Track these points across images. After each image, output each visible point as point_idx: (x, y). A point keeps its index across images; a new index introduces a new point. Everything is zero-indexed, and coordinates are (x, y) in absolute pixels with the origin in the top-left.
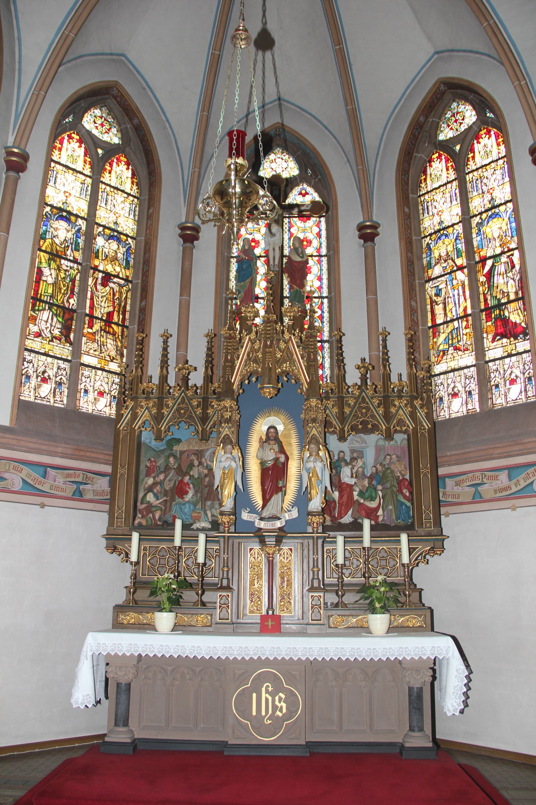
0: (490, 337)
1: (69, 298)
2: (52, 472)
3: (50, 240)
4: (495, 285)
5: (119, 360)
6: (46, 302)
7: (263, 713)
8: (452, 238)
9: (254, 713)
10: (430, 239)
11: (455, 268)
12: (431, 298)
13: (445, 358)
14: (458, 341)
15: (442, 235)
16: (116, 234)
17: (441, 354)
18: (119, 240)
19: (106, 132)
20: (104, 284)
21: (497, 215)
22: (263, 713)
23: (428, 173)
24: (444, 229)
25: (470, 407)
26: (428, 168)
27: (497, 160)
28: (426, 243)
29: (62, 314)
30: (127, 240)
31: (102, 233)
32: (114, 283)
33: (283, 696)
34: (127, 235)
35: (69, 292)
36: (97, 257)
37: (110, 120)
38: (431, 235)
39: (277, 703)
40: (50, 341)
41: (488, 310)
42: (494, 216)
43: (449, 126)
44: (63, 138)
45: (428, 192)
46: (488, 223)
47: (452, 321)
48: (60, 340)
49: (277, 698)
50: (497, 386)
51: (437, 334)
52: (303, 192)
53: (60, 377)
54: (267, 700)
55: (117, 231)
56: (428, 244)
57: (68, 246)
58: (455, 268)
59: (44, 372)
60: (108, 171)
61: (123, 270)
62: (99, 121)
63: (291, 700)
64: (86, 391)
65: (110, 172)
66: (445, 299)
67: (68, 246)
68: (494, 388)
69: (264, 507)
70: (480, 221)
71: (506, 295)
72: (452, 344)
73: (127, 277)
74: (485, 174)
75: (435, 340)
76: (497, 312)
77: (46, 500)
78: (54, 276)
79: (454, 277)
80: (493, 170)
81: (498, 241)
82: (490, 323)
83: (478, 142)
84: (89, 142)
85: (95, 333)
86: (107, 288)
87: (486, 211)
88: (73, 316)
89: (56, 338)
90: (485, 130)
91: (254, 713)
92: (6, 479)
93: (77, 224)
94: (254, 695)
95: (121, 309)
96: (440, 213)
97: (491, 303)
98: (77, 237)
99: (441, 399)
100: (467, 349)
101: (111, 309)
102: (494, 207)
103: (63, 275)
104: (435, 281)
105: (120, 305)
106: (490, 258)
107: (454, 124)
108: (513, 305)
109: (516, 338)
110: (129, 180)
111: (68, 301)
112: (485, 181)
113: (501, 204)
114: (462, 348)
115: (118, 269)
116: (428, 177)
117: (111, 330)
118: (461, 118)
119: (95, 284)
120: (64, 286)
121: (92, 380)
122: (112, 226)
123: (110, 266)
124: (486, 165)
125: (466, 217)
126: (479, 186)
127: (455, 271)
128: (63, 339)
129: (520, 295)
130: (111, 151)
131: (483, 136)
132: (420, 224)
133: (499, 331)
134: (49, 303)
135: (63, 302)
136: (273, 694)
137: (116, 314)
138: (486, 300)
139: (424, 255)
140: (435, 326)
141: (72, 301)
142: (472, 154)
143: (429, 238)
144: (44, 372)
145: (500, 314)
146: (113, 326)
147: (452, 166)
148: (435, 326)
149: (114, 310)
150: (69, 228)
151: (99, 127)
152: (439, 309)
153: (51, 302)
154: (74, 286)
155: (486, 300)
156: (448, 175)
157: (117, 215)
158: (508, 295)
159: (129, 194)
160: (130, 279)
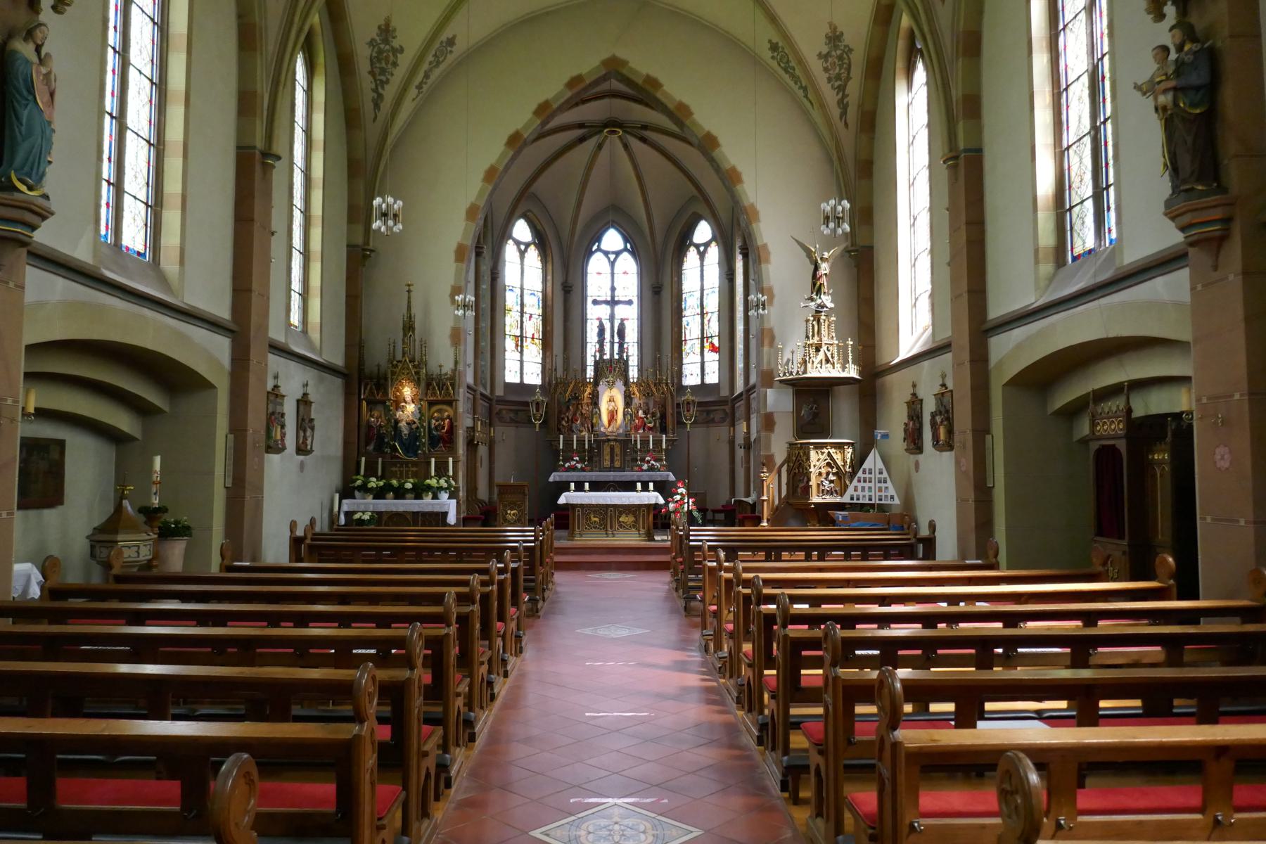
84: (518, 243)
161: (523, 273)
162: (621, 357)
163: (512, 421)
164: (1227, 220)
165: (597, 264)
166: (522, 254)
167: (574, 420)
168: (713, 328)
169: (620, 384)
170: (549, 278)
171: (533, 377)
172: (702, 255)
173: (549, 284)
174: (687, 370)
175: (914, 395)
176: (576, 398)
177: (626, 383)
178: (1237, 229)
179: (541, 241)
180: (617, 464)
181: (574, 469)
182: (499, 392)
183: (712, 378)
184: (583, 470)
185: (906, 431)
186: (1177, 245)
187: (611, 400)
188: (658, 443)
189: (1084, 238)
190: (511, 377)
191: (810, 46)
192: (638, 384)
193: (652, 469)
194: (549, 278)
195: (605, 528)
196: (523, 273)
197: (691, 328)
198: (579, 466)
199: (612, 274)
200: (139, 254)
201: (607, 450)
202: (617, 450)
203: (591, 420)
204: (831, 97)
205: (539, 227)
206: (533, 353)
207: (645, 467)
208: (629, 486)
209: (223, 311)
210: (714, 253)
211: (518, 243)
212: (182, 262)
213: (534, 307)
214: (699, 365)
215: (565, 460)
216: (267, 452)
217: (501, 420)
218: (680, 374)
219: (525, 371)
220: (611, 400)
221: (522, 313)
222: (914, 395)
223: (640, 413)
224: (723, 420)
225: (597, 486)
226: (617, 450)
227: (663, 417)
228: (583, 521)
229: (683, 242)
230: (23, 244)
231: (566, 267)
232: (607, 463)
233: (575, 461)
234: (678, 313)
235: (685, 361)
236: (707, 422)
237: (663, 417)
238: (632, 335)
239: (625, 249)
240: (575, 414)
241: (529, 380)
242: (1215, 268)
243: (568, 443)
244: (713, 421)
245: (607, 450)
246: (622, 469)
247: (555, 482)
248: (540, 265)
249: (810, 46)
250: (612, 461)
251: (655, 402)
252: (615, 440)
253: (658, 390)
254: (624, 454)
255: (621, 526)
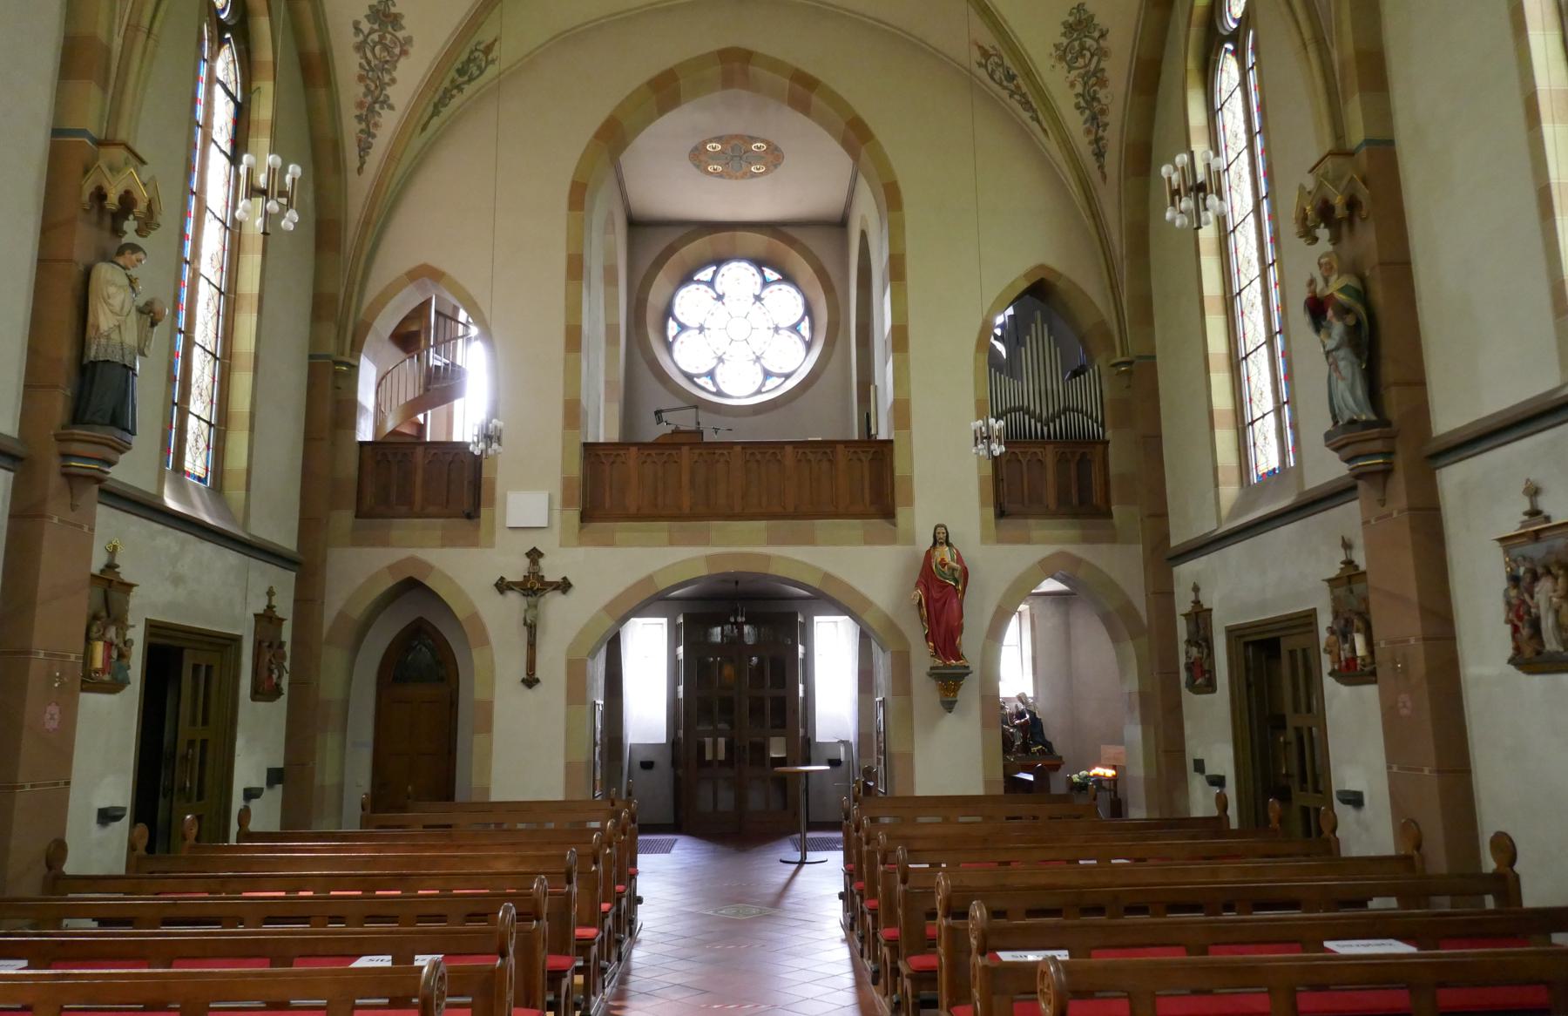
164: (1388, 454)
175: (1197, 602)
178: (1399, 461)
185: (1509, 603)
186: (1340, 478)
189: (1267, 457)
191: (1039, 39)
200: (199, 479)
204: (1075, 122)
209: (285, 537)
212: (248, 489)
216: (83, 690)
222: (1197, 602)
230: (99, 481)
242: (1383, 503)
249: (1039, 39)
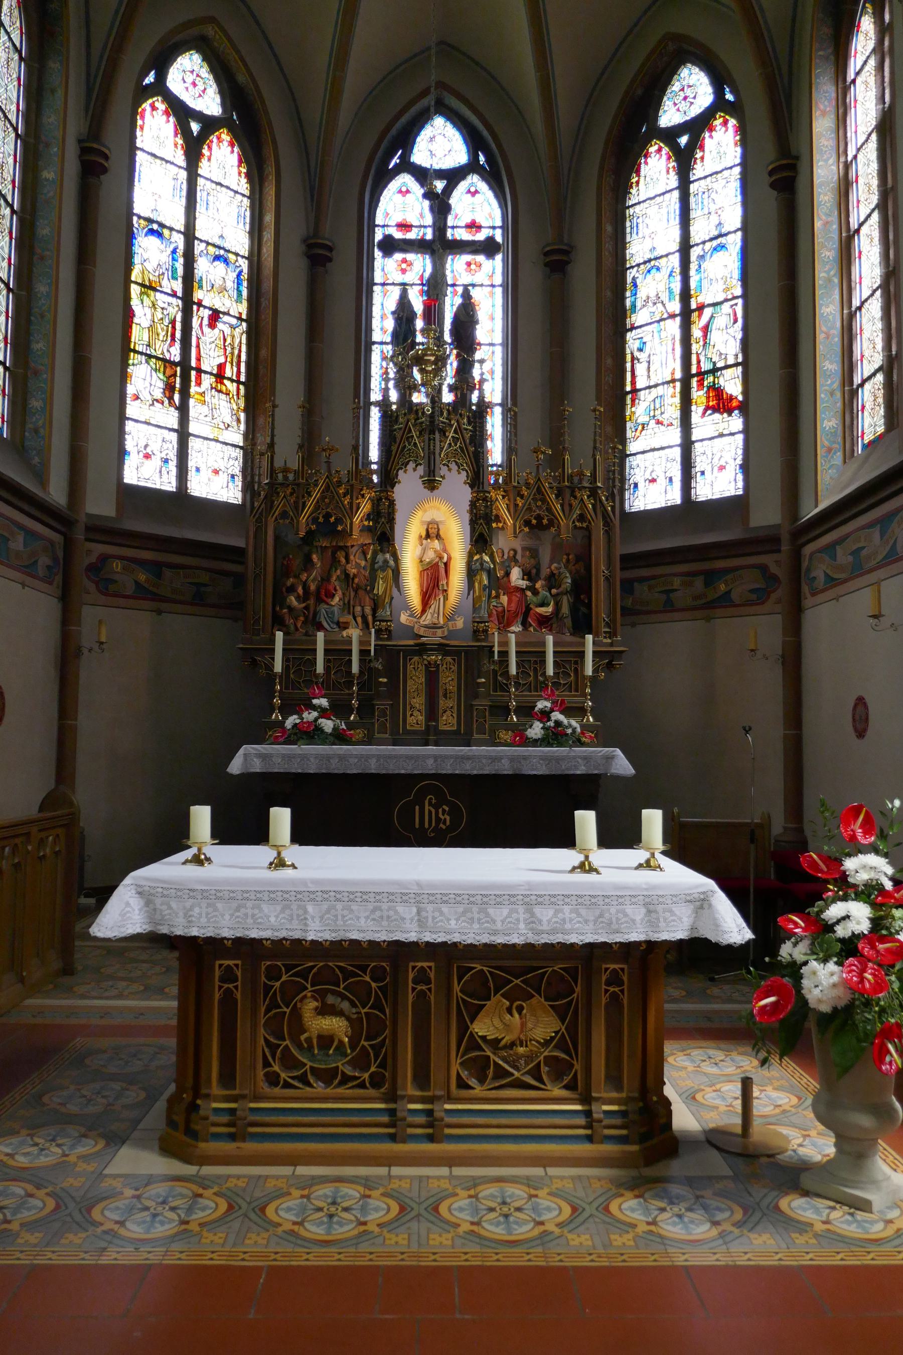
0: (701, 409)
1: (171, 346)
2: (168, 573)
3: (140, 266)
4: (712, 343)
5: (236, 427)
6: (141, 353)
7: (427, 826)
8: (665, 272)
9: (417, 826)
10: (638, 271)
11: (665, 316)
12: (632, 354)
13: (644, 432)
14: (662, 413)
15: (652, 268)
16: (222, 252)
17: (640, 428)
18: (226, 261)
19: (200, 96)
20: (212, 325)
21: (723, 246)
22: (427, 826)
23: (642, 173)
24: (656, 259)
25: (669, 496)
26: (643, 166)
27: (731, 168)
28: (632, 276)
29: (162, 369)
30: (237, 261)
31: (205, 252)
32: (225, 323)
33: (447, 809)
34: (237, 255)
35: (169, 338)
36: (201, 287)
37: (203, 76)
38: (638, 265)
39: (441, 816)
40: (150, 405)
41: (701, 374)
42: (719, 249)
43: (675, 104)
44: (144, 110)
45: (639, 203)
46: (711, 256)
47: (656, 386)
48: (162, 403)
49: (440, 810)
50: (703, 473)
51: (637, 401)
52: (473, 190)
53: (167, 451)
54: (430, 812)
55: (223, 248)
56: (634, 278)
57: (163, 274)
58: (665, 316)
59: (146, 446)
60: (206, 158)
61: (234, 303)
62: (190, 78)
63: (454, 812)
64: (198, 470)
65: (209, 159)
66: (649, 356)
67: (163, 274)
68: (699, 474)
69: (424, 611)
70: (702, 253)
71: (723, 357)
72: (654, 416)
73: (240, 314)
74: (715, 186)
75: (633, 409)
76: (711, 379)
77: (164, 606)
78: (149, 316)
79: (662, 327)
80: (725, 181)
81: (721, 282)
82: (701, 393)
83: (711, 137)
84: (180, 112)
85: (204, 392)
86: (216, 330)
87: (711, 239)
88: (176, 371)
89: (157, 401)
90: (721, 119)
91: (417, 826)
92: (116, 582)
93: (172, 240)
94: (417, 808)
95: (235, 360)
96: (653, 236)
97: (706, 366)
98: (173, 259)
99: (636, 485)
100: (671, 424)
101: (222, 360)
102: (721, 235)
103: (160, 316)
104: (639, 330)
105: (232, 354)
106: (709, 305)
107: (683, 102)
108: (730, 371)
109: (730, 415)
110: (236, 170)
111: (168, 351)
112: (713, 195)
113: (729, 233)
114: (665, 423)
115: (228, 303)
116: (642, 179)
117: (224, 388)
118: (692, 96)
119: (201, 325)
120: (162, 329)
121: (205, 455)
122: (218, 242)
123: (217, 298)
124: (717, 173)
125: (685, 247)
126: (706, 203)
127: (664, 319)
128: (166, 402)
129: (740, 360)
130: (210, 125)
131: (718, 128)
132: (625, 249)
133: (711, 404)
134: (146, 355)
135: (163, 353)
136: (436, 807)
137: (228, 366)
138: (699, 362)
139: (628, 294)
140: (635, 391)
141: (172, 349)
142: (701, 154)
143: (636, 268)
144: (146, 446)
145: (714, 382)
146: (225, 381)
147: (674, 167)
148: (635, 391)
149: (226, 361)
150: (163, 247)
151: (191, 88)
152: (640, 369)
153: (148, 352)
154: (174, 328)
155: (699, 362)
156: (668, 181)
157: (223, 224)
158: (726, 358)
159: (236, 192)
160: (244, 317)
161: (190, 200)
162: (462, 400)
163: (142, 593)
165: (400, 206)
166: (194, 150)
167: (323, 594)
168: (724, 340)
169: (455, 482)
170: (269, 218)
171: (217, 478)
172: (684, 162)
173: (268, 236)
174: (639, 469)
176: (330, 528)
177: (477, 479)
179: (245, 120)
180: (448, 721)
181: (311, 734)
182: (99, 505)
183: (721, 480)
184: (339, 737)
187: (432, 528)
188: (570, 660)
190: (146, 465)
192: (510, 488)
193: (555, 736)
194: (269, 218)
195: (384, 1083)
196: (190, 200)
197: (654, 352)
198: (328, 725)
199: (440, 227)
201: (416, 680)
202: (448, 679)
203: (371, 592)
205: (242, 78)
206: (219, 420)
207: (536, 730)
208: (528, 813)
210: (722, 147)
211: (180, 112)
213: (223, 288)
214: (677, 453)
215: (286, 711)
217: (107, 588)
218: (617, 481)
219: (192, 462)
220: (432, 533)
221: (188, 303)
223: (516, 576)
224: (759, 597)
225: (343, 813)
226: (448, 679)
227: (582, 588)
228: (254, 1036)
229: (632, 129)
231: (316, 194)
232: (416, 720)
233: (317, 713)
234: (615, 320)
235: (632, 447)
236: (711, 605)
237: (582, 588)
238: (490, 328)
239: (471, 167)
240: (326, 579)
241: (202, 486)
243: (300, 656)
244: (725, 601)
245: (416, 680)
246: (462, 738)
247: (247, 777)
248: (244, 186)
250: (432, 712)
251: (558, 548)
252: (442, 648)
253: (568, 508)
254: (469, 690)
255: (480, 1068)
